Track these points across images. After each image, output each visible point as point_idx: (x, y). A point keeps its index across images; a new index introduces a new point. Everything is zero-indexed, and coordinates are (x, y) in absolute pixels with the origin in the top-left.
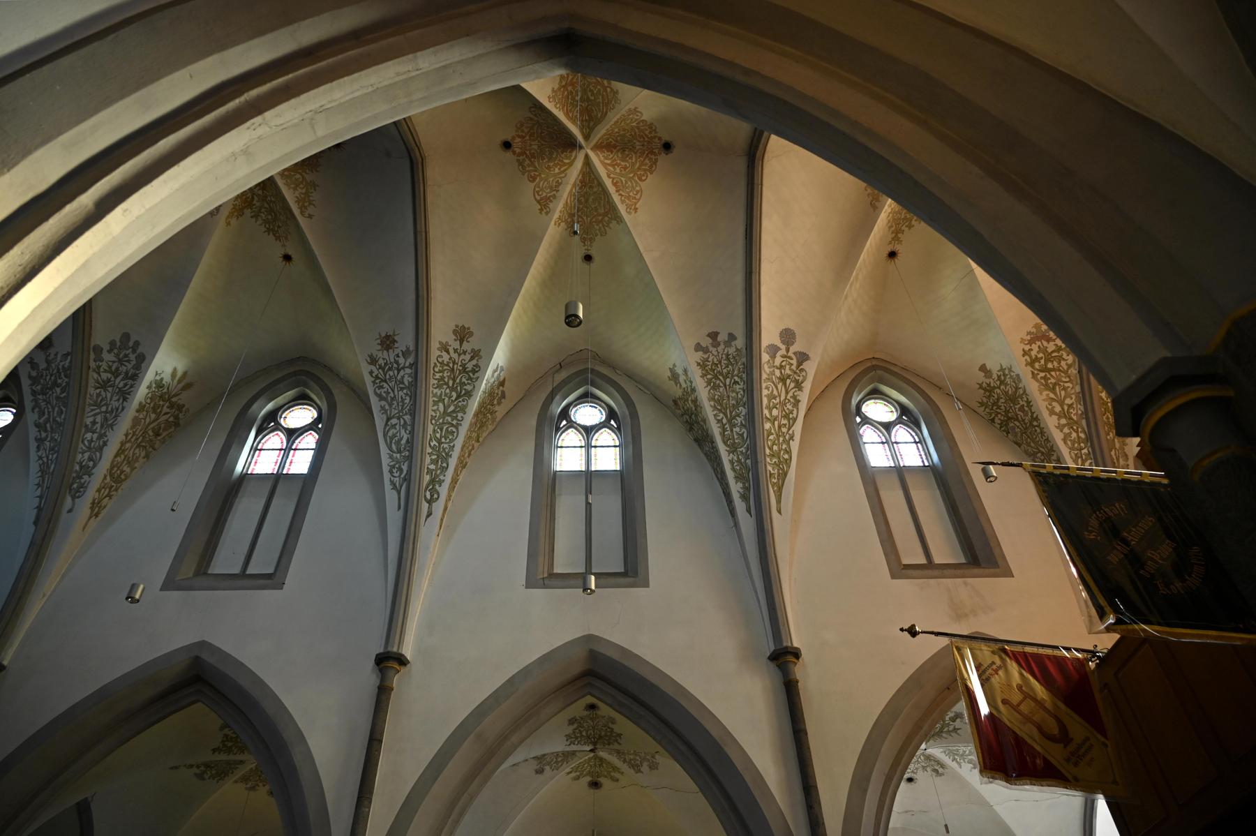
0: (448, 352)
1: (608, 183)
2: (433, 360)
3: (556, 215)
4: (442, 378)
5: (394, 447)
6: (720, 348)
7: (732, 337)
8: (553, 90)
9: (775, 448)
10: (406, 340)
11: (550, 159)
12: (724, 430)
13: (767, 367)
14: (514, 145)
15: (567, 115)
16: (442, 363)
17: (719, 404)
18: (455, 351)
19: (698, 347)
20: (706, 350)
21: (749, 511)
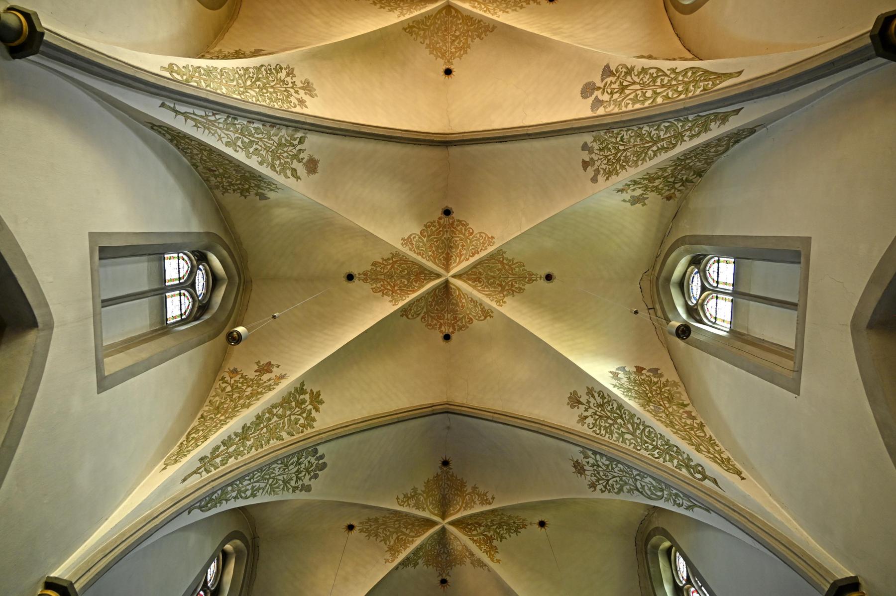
0: (586, 417)
1: (472, 260)
2: (590, 432)
3: (494, 304)
4: (605, 428)
5: (659, 494)
6: (595, 157)
7: (585, 147)
8: (390, 301)
9: (680, 89)
10: (576, 453)
11: (457, 305)
12: (663, 148)
13: (614, 107)
14: (447, 332)
15: (414, 291)
16: (594, 425)
17: (641, 155)
18: (586, 410)
19: (594, 180)
20: (597, 172)
21: (737, 112)
